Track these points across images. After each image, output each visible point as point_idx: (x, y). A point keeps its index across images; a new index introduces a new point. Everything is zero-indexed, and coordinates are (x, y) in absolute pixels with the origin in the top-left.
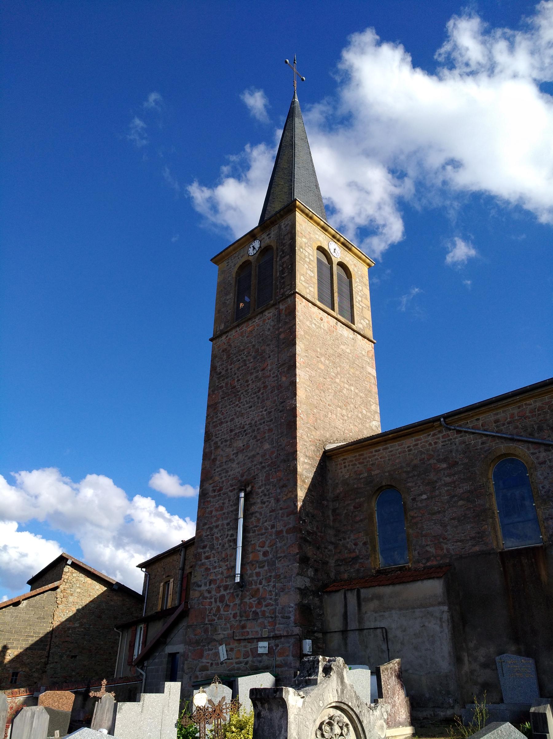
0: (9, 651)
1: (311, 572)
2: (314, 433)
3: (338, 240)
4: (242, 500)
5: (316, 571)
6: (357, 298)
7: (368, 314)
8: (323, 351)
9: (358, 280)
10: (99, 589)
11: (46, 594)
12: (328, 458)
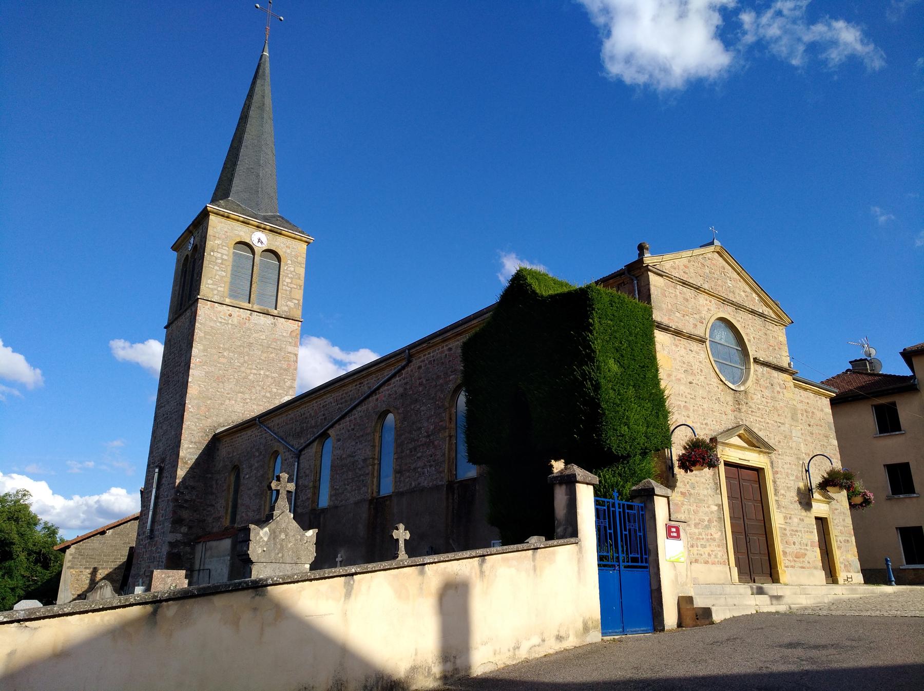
0: (100, 571)
1: (184, 529)
2: (203, 422)
3: (264, 229)
4: (156, 475)
5: (190, 528)
6: (285, 280)
7: (299, 294)
8: (227, 346)
9: (289, 262)
10: (672, 428)
11: (129, 523)
12: (216, 441)
